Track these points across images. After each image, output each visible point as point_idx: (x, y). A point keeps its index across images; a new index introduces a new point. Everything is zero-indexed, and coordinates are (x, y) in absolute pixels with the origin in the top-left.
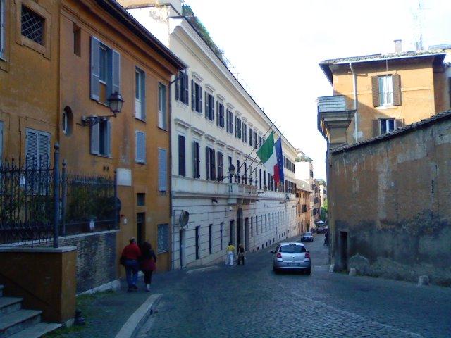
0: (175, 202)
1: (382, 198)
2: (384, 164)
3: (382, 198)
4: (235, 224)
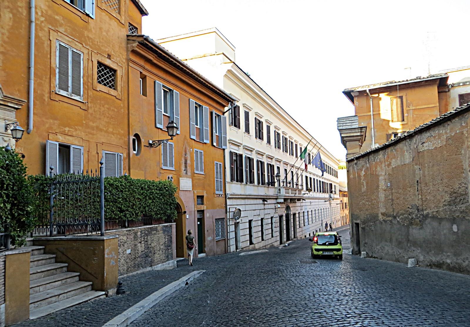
0: (229, 202)
1: (382, 196)
2: (382, 167)
3: (382, 196)
4: (284, 218)
